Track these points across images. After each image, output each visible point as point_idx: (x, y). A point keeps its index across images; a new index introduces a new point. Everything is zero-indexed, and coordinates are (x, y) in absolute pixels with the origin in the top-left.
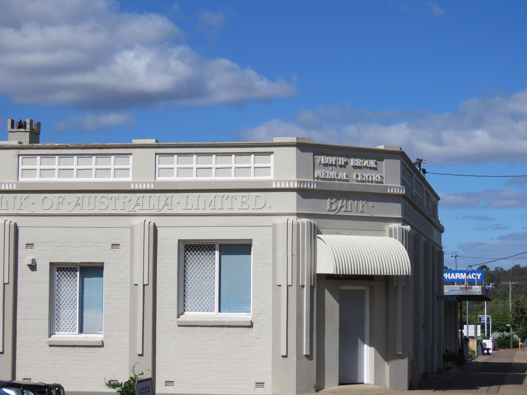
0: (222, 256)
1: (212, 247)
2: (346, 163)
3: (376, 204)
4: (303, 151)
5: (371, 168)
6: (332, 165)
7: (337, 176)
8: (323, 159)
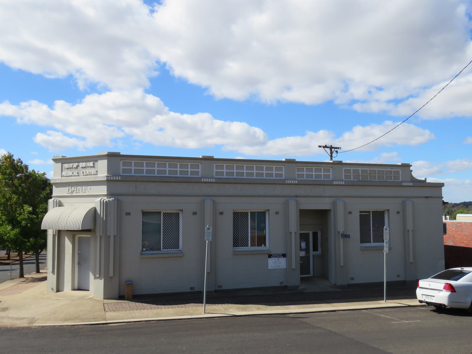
0: (336, 278)
1: (151, 220)
2: (78, 166)
3: (92, 187)
4: (56, 163)
5: (91, 167)
6: (70, 168)
7: (73, 173)
8: (66, 166)
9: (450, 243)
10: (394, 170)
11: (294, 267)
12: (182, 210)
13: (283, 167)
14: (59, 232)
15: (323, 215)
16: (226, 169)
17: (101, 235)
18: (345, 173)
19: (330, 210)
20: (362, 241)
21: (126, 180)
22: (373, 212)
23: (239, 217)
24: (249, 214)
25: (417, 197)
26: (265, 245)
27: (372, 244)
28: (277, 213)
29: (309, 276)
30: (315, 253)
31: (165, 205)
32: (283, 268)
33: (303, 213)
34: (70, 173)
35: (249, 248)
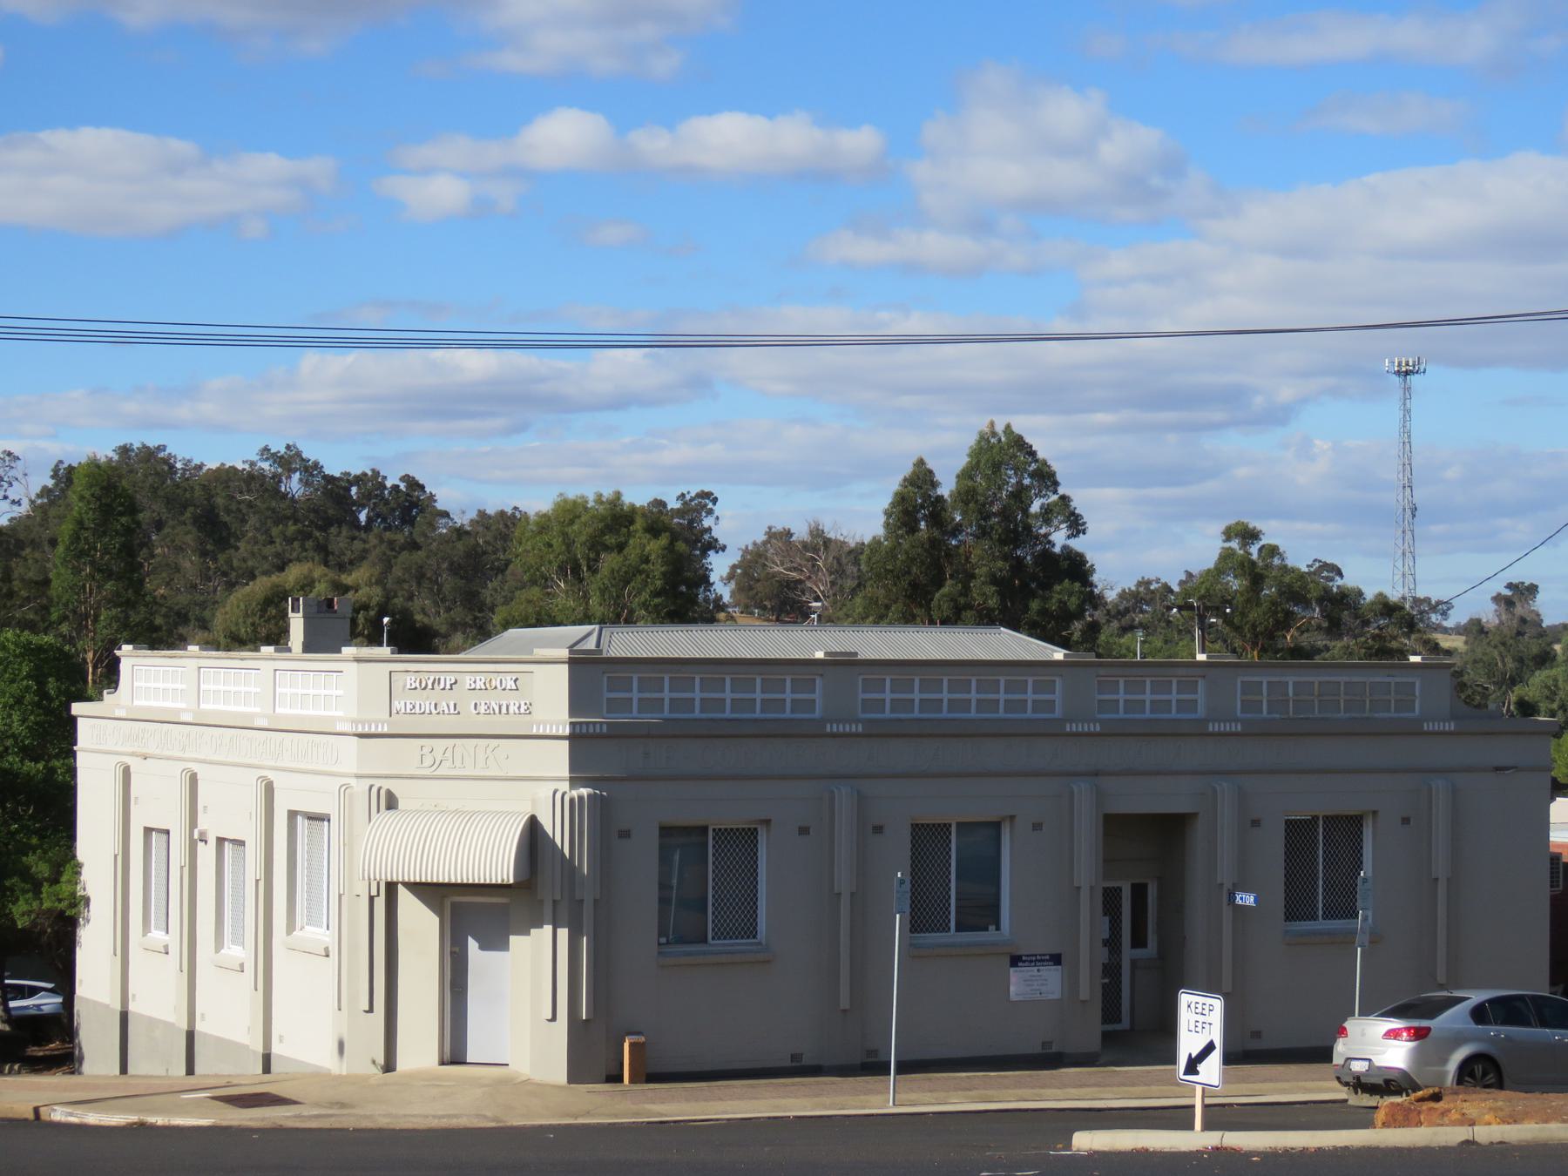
9: (559, 1074)
10: (1398, 679)
11: (1084, 993)
12: (767, 822)
13: (1058, 680)
14: (391, 888)
15: (1169, 831)
16: (892, 692)
17: (558, 897)
18: (1244, 693)
19: (1194, 815)
20: (1290, 916)
21: (616, 734)
22: (1326, 818)
23: (927, 838)
24: (953, 829)
25: (1469, 770)
26: (998, 929)
27: (1321, 924)
28: (1037, 827)
29: (1117, 1027)
30: (1139, 952)
31: (720, 808)
32: (1051, 997)
33: (1116, 826)
34: (425, 702)
35: (953, 936)
